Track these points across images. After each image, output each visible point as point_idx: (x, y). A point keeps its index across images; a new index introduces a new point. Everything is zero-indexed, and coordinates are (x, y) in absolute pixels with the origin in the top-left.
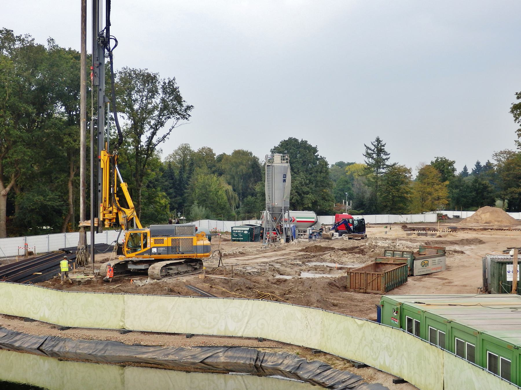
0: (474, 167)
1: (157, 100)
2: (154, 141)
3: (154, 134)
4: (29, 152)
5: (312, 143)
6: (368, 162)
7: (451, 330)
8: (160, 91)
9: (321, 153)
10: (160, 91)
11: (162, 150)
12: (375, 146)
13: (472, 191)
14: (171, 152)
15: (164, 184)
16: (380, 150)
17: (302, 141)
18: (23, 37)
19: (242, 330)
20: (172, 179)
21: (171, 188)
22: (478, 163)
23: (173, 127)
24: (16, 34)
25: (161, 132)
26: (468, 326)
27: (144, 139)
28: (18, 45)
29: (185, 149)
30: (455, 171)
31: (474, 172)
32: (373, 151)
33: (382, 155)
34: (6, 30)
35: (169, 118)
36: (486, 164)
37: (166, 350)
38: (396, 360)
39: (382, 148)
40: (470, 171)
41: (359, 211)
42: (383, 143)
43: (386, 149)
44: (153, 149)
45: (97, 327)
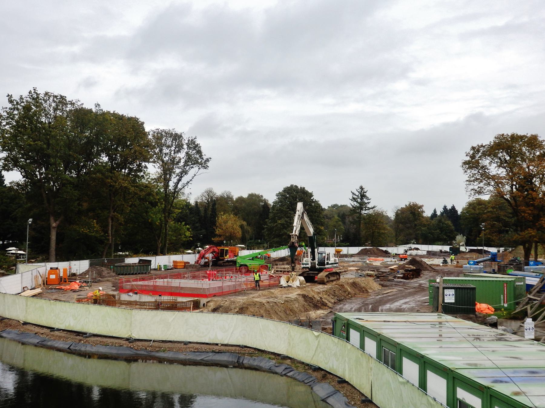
0: (442, 210)
1: (182, 155)
2: (180, 186)
3: (179, 180)
4: (76, 193)
5: (309, 189)
6: (353, 205)
7: (380, 341)
8: (185, 147)
9: (315, 197)
10: (185, 147)
11: (191, 193)
12: (359, 192)
13: (437, 229)
14: (199, 194)
15: (192, 219)
16: (363, 196)
17: (301, 188)
18: (74, 101)
19: (228, 339)
20: (199, 216)
21: (197, 223)
22: (445, 207)
23: (195, 175)
24: (68, 99)
25: (185, 179)
26: (391, 338)
27: (171, 184)
28: (69, 108)
29: (209, 192)
30: (424, 213)
31: (442, 214)
32: (358, 196)
33: (364, 199)
34: (61, 96)
35: (192, 167)
36: (452, 208)
37: (200, 353)
38: (341, 365)
39: (365, 194)
40: (438, 213)
41: (346, 244)
42: (365, 190)
43: (367, 194)
44: (178, 192)
45: (111, 335)
